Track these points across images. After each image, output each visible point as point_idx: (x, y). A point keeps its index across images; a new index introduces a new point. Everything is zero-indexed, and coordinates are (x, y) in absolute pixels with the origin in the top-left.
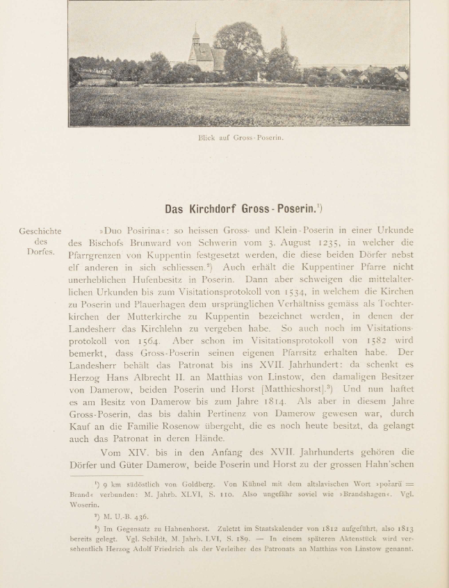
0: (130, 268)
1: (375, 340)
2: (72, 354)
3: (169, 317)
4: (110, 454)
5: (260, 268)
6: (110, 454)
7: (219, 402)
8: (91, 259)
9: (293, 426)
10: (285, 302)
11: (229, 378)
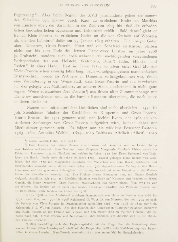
0: (63, 204)
3: (74, 21)
5: (108, 41)
9: (74, 56)
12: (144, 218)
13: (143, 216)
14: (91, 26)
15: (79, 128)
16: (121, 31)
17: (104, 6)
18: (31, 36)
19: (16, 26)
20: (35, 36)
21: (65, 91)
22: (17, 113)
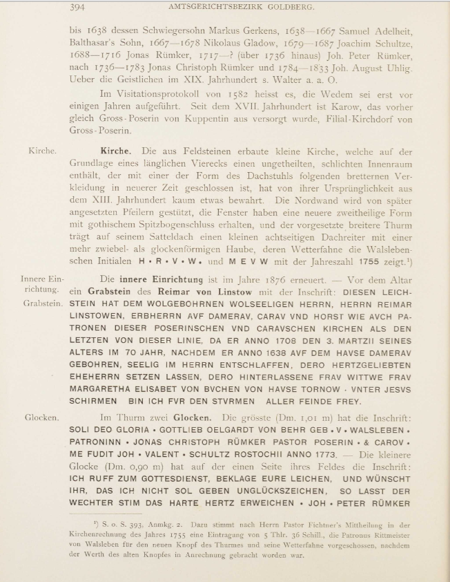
1: (237, 94)
2: (231, 201)
4: (357, 281)
6: (357, 281)
7: (154, 418)
8: (274, 167)
10: (402, 175)
11: (174, 164)
13: (111, 555)
15: (305, 177)
16: (73, 43)
21: (299, 199)
22: (338, 69)
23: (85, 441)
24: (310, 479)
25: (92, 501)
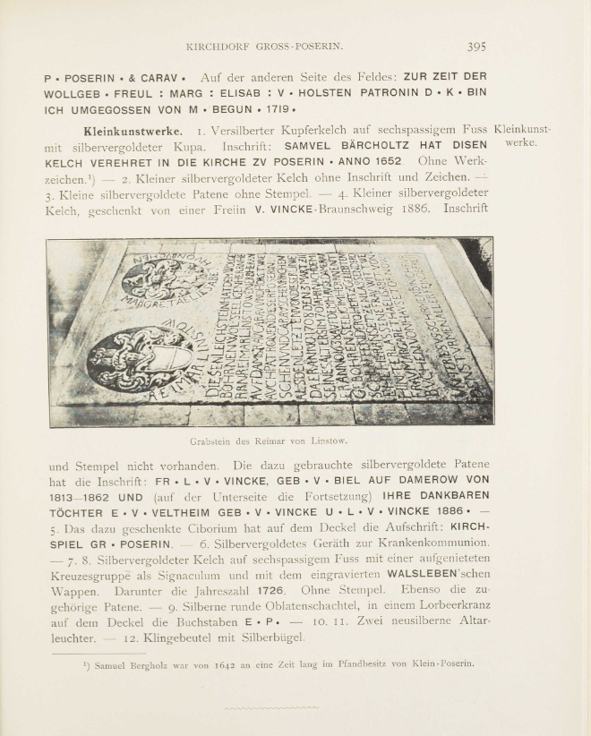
12: (227, 644)
14: (431, 177)
17: (324, 46)
18: (145, 181)
19: (156, 213)
20: (158, 180)
23: (380, 92)
24: (55, 110)
25: (76, 511)
